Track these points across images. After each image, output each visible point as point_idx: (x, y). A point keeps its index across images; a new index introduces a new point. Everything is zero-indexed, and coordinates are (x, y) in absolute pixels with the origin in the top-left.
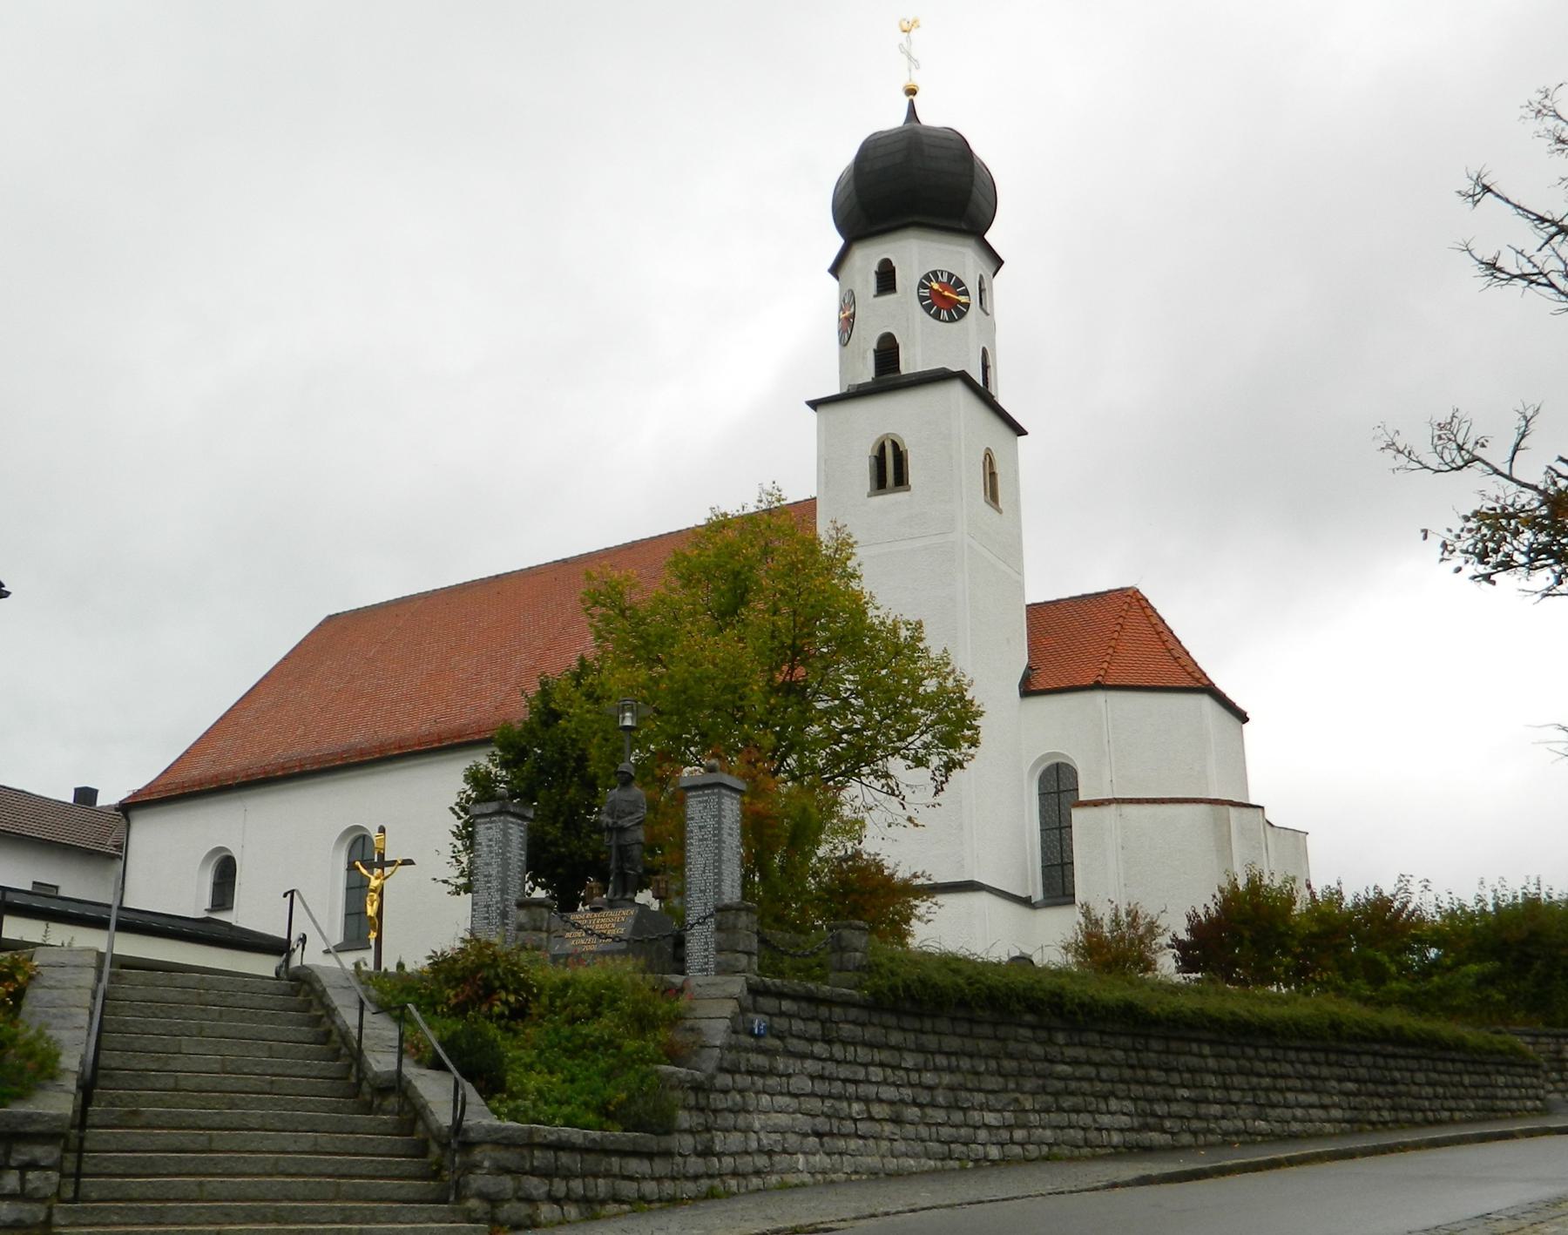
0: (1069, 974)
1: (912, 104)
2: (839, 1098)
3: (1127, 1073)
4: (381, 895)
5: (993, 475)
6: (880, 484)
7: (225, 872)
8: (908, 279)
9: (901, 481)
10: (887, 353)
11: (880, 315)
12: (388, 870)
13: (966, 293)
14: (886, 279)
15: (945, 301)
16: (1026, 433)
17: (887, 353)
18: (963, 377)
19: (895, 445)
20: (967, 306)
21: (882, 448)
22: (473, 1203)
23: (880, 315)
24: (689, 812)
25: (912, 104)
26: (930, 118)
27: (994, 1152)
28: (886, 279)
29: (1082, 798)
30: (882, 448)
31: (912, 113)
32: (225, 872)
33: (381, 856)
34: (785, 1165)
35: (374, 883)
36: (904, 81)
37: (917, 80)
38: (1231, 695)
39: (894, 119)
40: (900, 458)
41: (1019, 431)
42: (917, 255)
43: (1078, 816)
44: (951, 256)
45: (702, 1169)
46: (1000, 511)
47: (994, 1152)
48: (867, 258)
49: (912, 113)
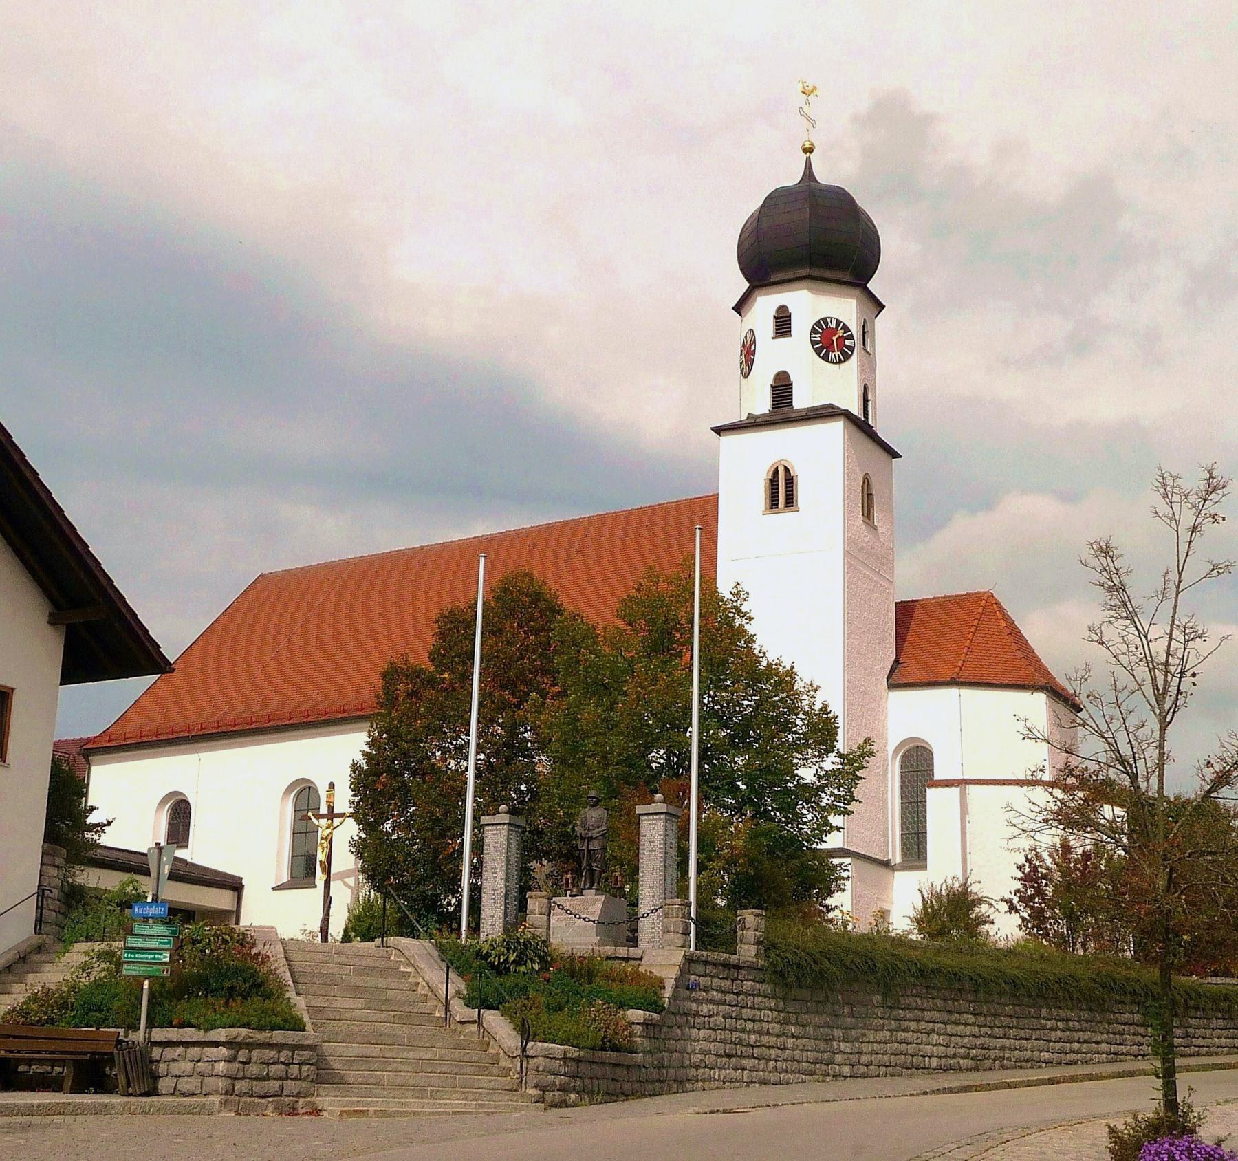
0: (913, 945)
1: (808, 161)
2: (743, 1031)
3: (945, 1016)
4: (330, 842)
5: (870, 495)
6: (773, 503)
7: (180, 814)
8: (802, 326)
9: (790, 502)
10: (782, 389)
11: (774, 355)
12: (336, 821)
13: (851, 337)
14: (783, 324)
15: (830, 342)
16: (898, 456)
17: (782, 389)
18: (847, 415)
19: (786, 469)
20: (852, 349)
21: (776, 472)
22: (531, 1091)
23: (774, 355)
24: (642, 831)
25: (808, 161)
26: (824, 176)
27: (846, 1070)
28: (783, 324)
29: (938, 776)
30: (776, 472)
31: (808, 173)
32: (180, 814)
33: (331, 808)
34: (706, 1076)
35: (323, 832)
36: (803, 139)
37: (818, 140)
38: (1011, 787)
39: (792, 178)
40: (790, 482)
41: (895, 455)
42: (809, 304)
43: (931, 793)
44: (843, 308)
45: (656, 1077)
46: (875, 528)
47: (846, 1070)
48: (766, 305)
49: (808, 173)
